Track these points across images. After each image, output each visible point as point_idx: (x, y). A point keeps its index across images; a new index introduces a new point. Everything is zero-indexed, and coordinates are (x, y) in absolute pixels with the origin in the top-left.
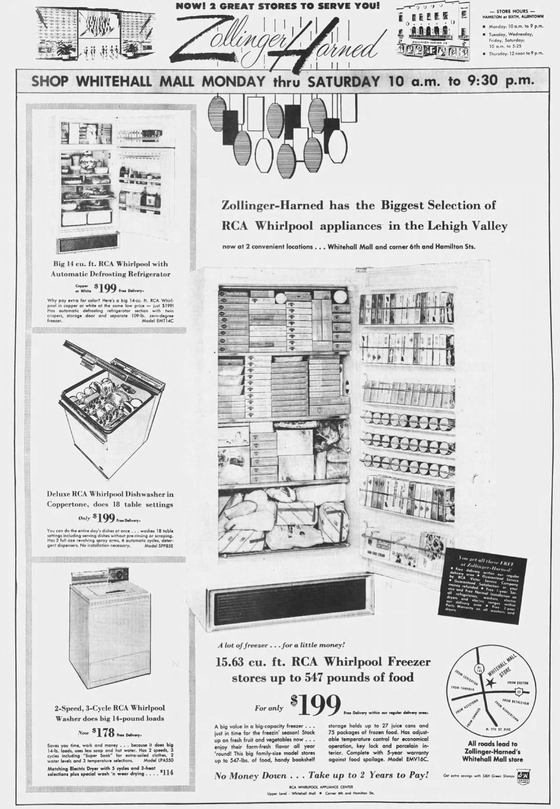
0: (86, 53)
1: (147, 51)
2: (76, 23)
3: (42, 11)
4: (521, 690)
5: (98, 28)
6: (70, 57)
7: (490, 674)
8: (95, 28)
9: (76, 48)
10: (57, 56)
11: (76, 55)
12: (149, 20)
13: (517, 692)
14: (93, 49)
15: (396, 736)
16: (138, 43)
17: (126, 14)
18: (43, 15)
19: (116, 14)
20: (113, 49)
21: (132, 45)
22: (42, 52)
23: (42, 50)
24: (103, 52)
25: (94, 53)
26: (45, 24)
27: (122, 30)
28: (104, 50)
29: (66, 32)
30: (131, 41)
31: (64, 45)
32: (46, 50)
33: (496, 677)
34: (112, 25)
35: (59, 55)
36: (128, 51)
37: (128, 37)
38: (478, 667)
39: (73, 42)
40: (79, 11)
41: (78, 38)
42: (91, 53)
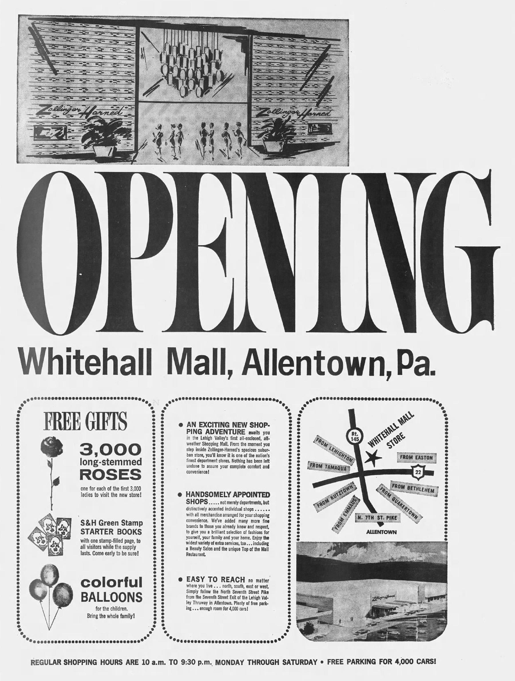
0: (159, 143)
1: (319, 139)
2: (133, 62)
3: (44, 28)
4: (421, 469)
5: (190, 73)
6: (116, 153)
7: (371, 444)
8: (183, 75)
9: (133, 127)
10: (82, 150)
11: (133, 148)
12: (324, 56)
13: (415, 472)
14: (177, 131)
15: (245, 595)
16: (294, 117)
17: (264, 40)
18: (47, 41)
19: (238, 40)
20: (230, 131)
21: (279, 120)
22: (44, 138)
23: (43, 133)
24: (204, 141)
25: (180, 141)
26: (51, 63)
27: (254, 82)
28: (204, 133)
29: (106, 85)
30: (276, 112)
31: (102, 121)
32: (54, 132)
33: (381, 448)
34: (227, 67)
35: (85, 147)
36: (271, 139)
37: (269, 100)
38: (353, 434)
39: (125, 112)
40: (142, 29)
41: (137, 102)
42: (172, 141)
